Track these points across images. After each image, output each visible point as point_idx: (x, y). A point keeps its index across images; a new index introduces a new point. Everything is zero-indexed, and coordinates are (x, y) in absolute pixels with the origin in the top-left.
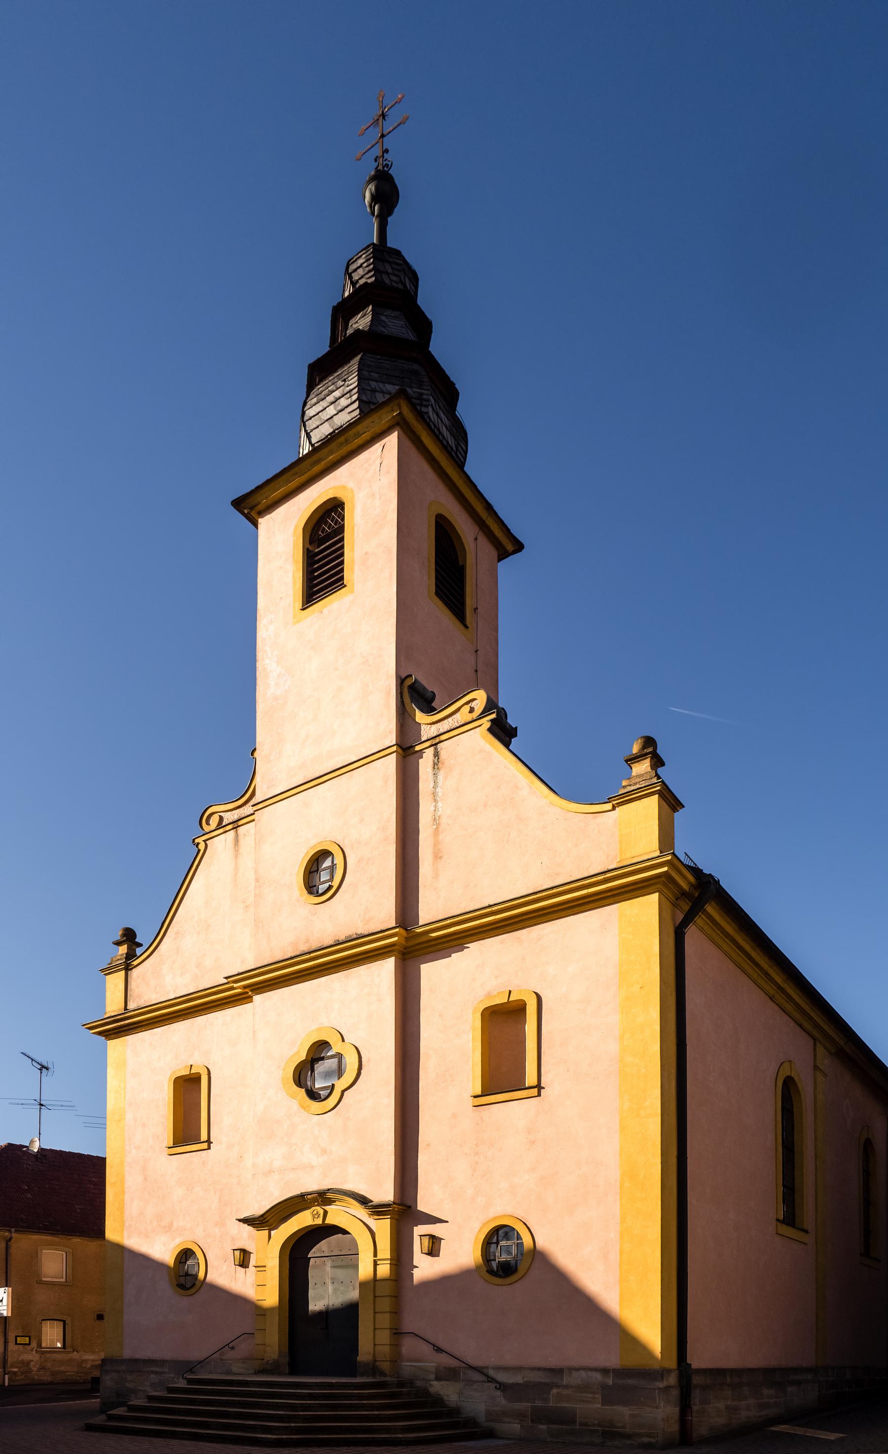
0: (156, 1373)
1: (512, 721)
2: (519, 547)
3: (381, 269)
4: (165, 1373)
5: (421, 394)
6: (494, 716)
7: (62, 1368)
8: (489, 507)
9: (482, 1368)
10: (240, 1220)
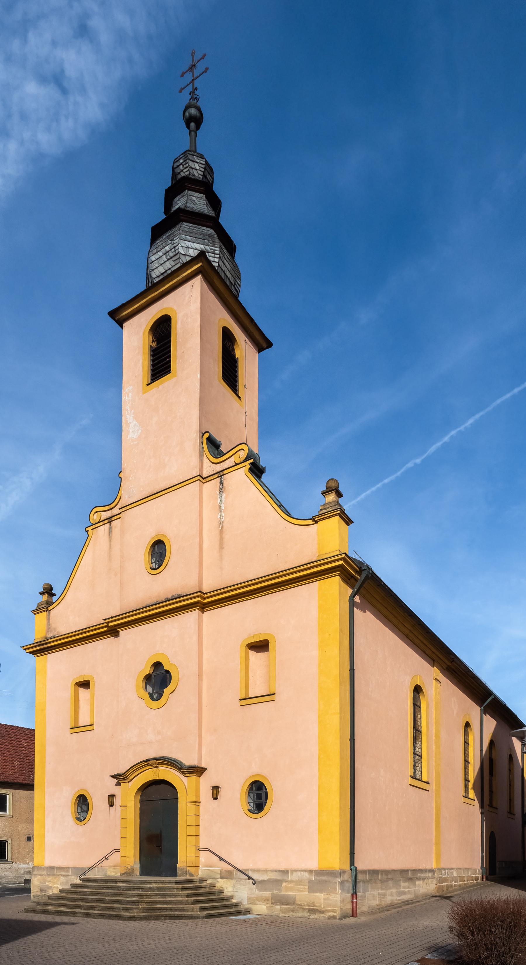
0: (64, 876)
1: (262, 464)
2: (269, 344)
3: (193, 167)
4: (68, 876)
5: (215, 250)
6: (252, 461)
7: (6, 874)
8: (252, 320)
9: (246, 870)
10: (112, 776)
